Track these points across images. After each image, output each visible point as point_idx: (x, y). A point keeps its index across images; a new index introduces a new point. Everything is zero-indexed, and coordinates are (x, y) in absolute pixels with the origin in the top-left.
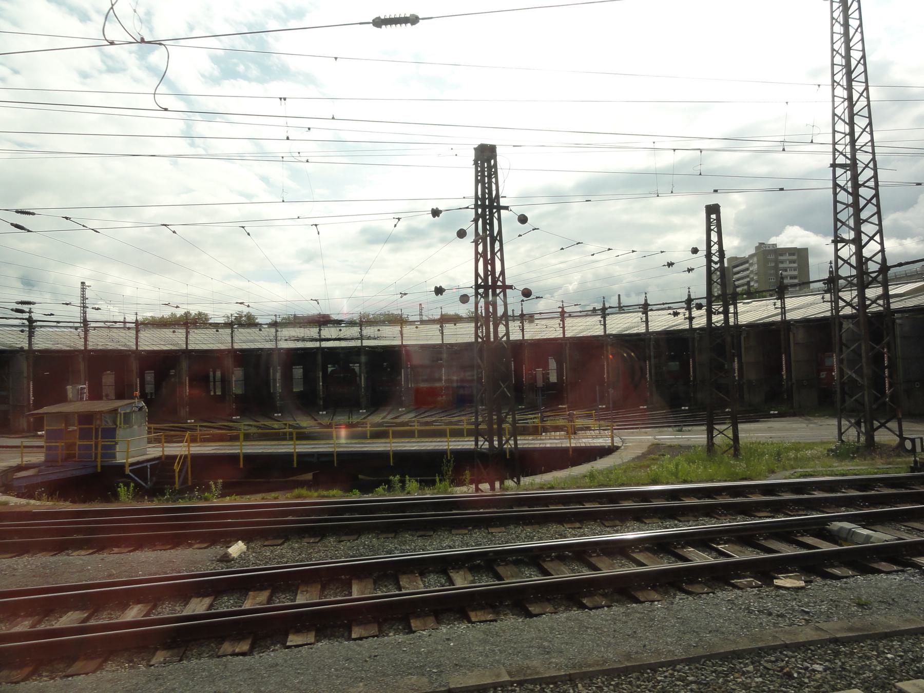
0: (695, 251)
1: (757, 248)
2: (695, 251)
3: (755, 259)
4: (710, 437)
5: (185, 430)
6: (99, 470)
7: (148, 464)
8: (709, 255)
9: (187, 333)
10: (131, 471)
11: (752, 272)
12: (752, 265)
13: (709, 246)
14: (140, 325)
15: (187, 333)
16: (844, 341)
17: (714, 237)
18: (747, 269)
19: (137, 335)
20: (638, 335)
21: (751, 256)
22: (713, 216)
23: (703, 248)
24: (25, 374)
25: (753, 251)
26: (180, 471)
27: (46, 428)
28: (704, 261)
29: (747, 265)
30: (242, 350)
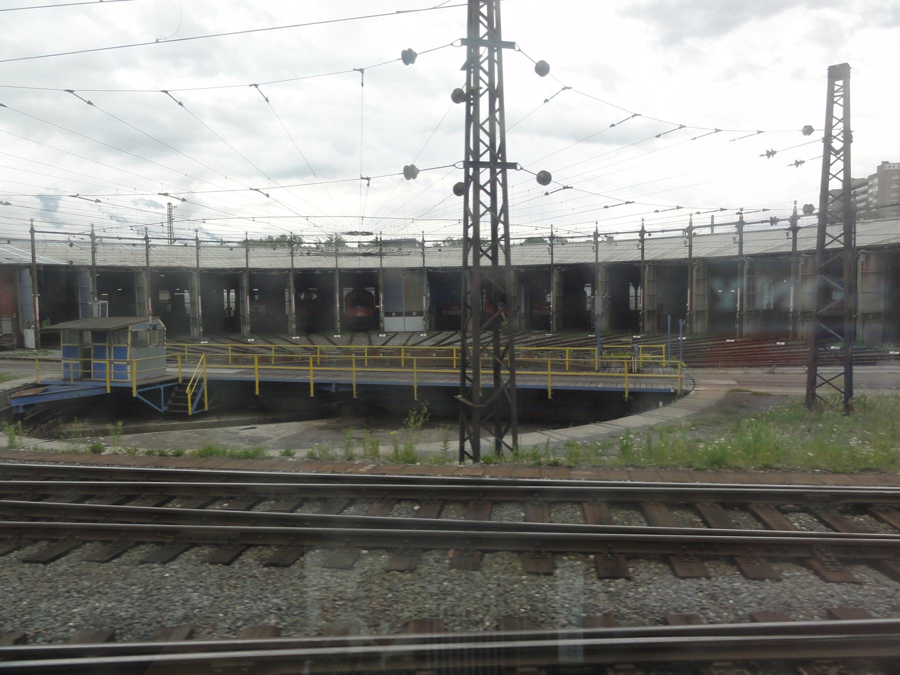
0: (808, 130)
1: (879, 168)
2: (808, 130)
3: (876, 180)
4: (812, 384)
5: (201, 351)
6: (109, 391)
7: (162, 387)
8: (828, 139)
9: (247, 251)
10: (139, 393)
11: (871, 195)
12: (871, 187)
13: (829, 127)
14: (247, 244)
15: (247, 251)
16: (469, 303)
17: (838, 112)
18: (865, 192)
19: (197, 252)
20: (730, 257)
21: (871, 177)
22: (840, 83)
23: (819, 125)
24: (91, 290)
25: (875, 172)
26: (194, 395)
27: (62, 345)
28: (820, 147)
29: (866, 187)
30: (46, 267)
